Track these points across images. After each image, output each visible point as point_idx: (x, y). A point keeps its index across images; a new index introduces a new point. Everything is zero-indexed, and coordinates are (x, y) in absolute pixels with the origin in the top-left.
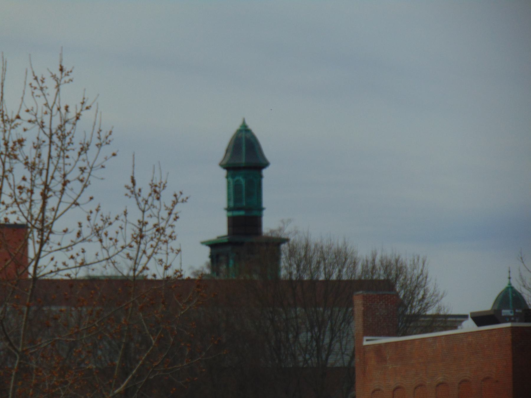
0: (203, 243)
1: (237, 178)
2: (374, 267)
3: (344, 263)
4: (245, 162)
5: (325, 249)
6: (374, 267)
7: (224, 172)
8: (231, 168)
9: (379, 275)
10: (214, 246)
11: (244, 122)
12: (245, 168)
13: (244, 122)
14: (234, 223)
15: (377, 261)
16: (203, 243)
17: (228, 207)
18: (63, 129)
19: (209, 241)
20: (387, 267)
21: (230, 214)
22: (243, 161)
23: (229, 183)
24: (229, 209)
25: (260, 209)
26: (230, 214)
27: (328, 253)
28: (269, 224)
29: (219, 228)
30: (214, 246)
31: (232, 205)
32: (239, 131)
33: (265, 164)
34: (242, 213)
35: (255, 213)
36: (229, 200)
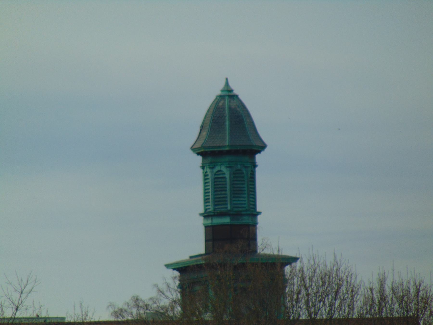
0: (168, 266)
1: (218, 168)
2: (383, 298)
3: (337, 293)
4: (230, 144)
5: (308, 274)
6: (383, 298)
7: (199, 159)
8: (208, 153)
9: (392, 310)
10: (183, 269)
11: (227, 84)
12: (228, 153)
13: (227, 84)
14: (215, 236)
15: (388, 291)
16: (168, 266)
17: (206, 210)
18: (141, 304)
19: (177, 263)
20: (403, 299)
21: (209, 222)
22: (226, 141)
23: (205, 175)
24: (206, 215)
25: (255, 214)
26: (209, 222)
27: (359, 286)
28: (271, 238)
29: (193, 244)
30: (183, 269)
31: (211, 208)
32: (221, 97)
33: (262, 147)
34: (226, 220)
35: (246, 220)
36: (206, 201)
